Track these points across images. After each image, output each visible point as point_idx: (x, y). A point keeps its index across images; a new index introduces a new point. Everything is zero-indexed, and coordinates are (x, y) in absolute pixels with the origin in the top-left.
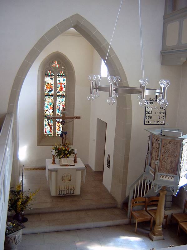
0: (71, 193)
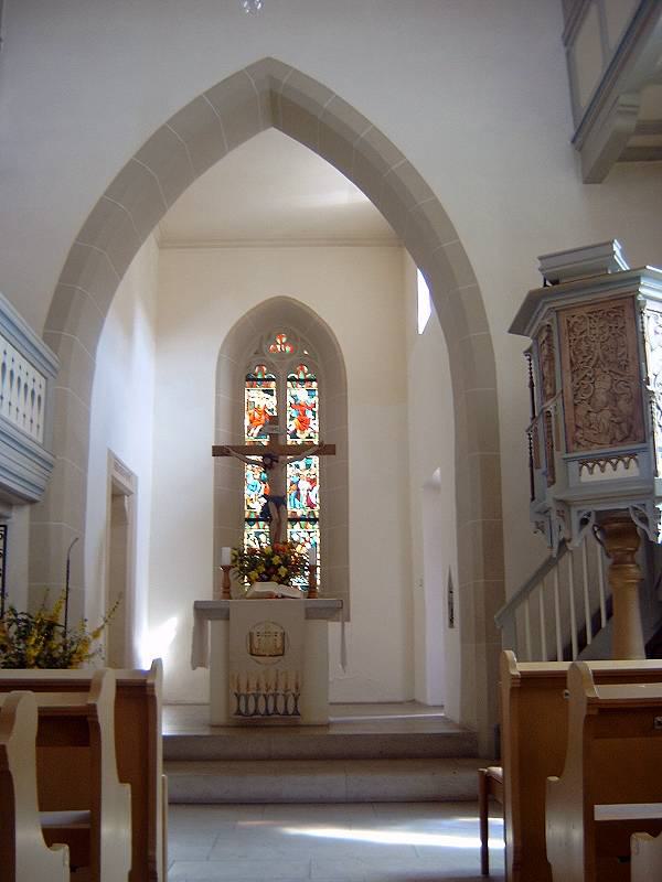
0: (286, 713)
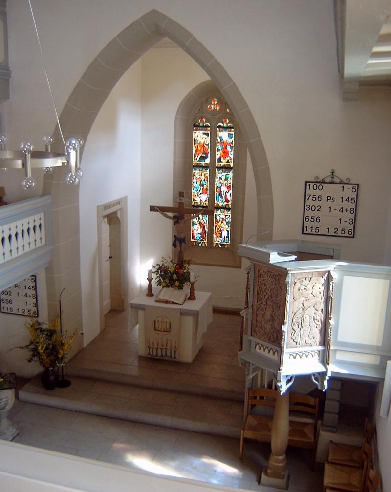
0: (157, 355)
